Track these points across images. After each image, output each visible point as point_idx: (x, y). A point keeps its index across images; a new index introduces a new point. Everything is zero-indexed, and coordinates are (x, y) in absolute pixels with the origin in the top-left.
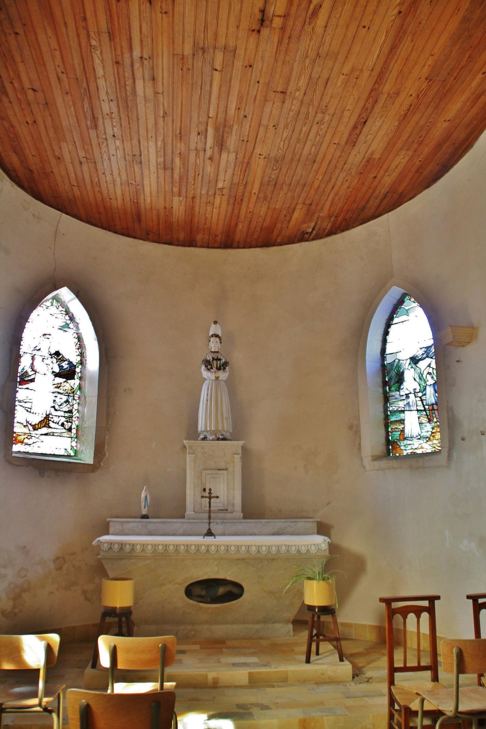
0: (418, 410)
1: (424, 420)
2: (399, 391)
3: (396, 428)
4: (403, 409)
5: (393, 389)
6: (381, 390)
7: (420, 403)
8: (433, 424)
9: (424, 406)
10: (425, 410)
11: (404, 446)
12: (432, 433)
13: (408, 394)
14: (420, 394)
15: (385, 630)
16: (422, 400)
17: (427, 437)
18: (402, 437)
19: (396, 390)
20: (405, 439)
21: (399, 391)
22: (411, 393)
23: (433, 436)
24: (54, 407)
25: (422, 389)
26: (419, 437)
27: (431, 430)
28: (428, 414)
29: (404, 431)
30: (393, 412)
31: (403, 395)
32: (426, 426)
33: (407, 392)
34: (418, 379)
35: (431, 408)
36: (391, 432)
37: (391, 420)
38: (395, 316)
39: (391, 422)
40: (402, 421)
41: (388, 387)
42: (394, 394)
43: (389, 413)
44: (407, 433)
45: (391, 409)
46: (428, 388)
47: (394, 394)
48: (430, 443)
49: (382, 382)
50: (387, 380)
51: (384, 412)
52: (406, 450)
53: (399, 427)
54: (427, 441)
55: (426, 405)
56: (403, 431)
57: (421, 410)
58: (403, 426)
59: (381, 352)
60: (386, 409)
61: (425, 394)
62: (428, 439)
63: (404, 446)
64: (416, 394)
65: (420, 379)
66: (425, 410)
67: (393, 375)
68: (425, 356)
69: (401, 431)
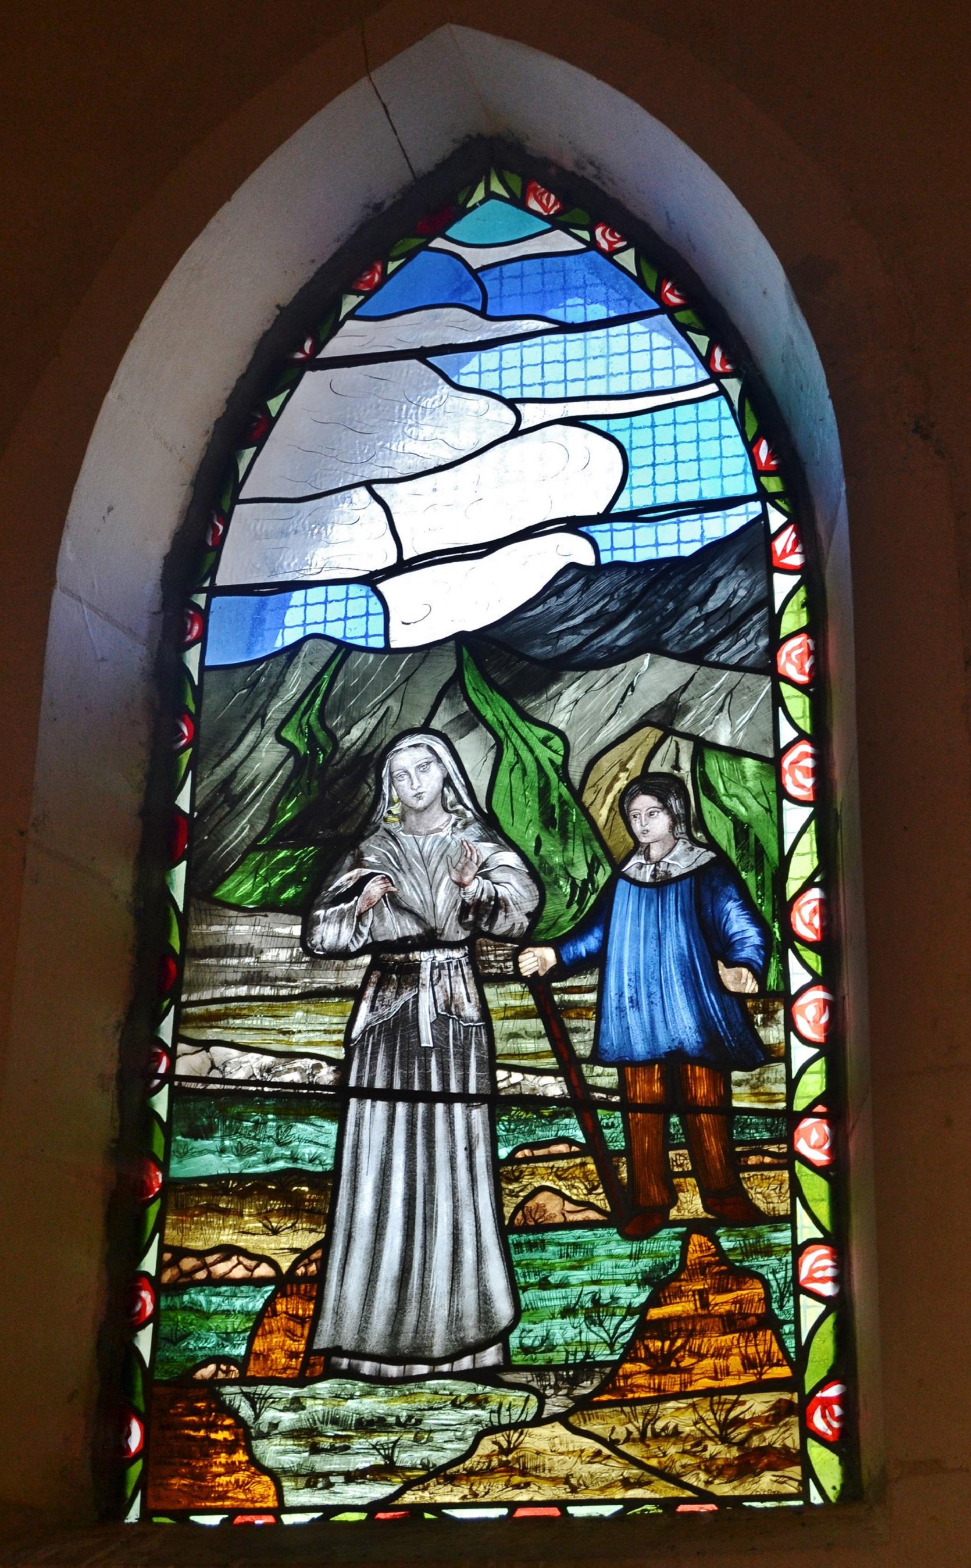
0: (497, 1103)
1: (563, 1191)
2: (304, 910)
3: (228, 1251)
4: (326, 1075)
5: (242, 887)
6: (122, 879)
7: (529, 1039)
8: (665, 1244)
9: (568, 1065)
10: (580, 1102)
11: (307, 1436)
12: (645, 1329)
13: (405, 944)
14: (537, 960)
15: (401, 1063)
16: (553, 1017)
17: (586, 1368)
18: (279, 1346)
19: (269, 905)
20: (318, 1364)
21: (304, 910)
22: (431, 939)
23: (660, 1364)
24: (257, 537)
25: (562, 912)
26: (491, 1357)
27: (636, 1296)
28: (615, 1137)
29: (320, 1280)
30: (216, 1105)
31: (344, 954)
32: (580, 1256)
33: (396, 927)
34: (524, 827)
35: (649, 1087)
36: (155, 1284)
37: (180, 1169)
38: (350, 302)
39: (171, 1185)
40: (307, 1197)
41: (180, 873)
42: (242, 931)
43: (161, 1103)
44: (355, 1301)
45: (189, 1063)
46: (627, 915)
47: (242, 931)
48: (608, 1423)
49: (144, 813)
50: (183, 801)
51: (122, 1078)
52: (313, 1479)
53: (265, 1244)
54: (584, 1405)
55: (597, 1057)
56: (304, 1283)
57: (535, 1103)
58: (305, 1240)
59: (170, 562)
60: (139, 1062)
61: (598, 960)
62: (585, 1388)
63: (307, 1436)
64: (495, 957)
65: (547, 820)
66: (580, 1102)
67: (247, 775)
68: (621, 634)
69: (284, 1283)
